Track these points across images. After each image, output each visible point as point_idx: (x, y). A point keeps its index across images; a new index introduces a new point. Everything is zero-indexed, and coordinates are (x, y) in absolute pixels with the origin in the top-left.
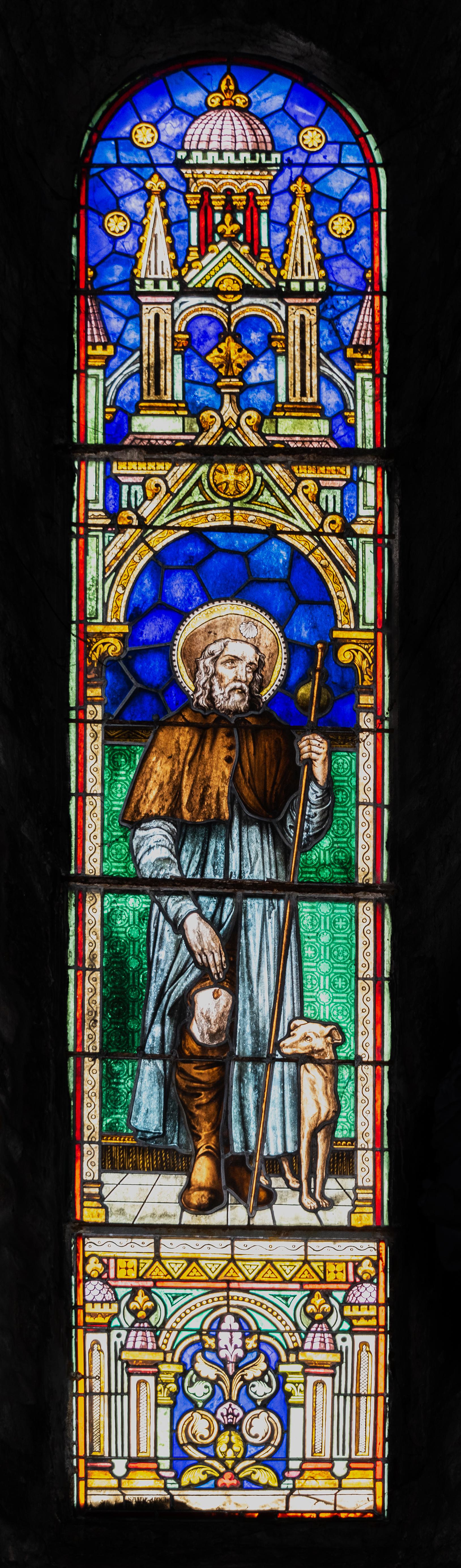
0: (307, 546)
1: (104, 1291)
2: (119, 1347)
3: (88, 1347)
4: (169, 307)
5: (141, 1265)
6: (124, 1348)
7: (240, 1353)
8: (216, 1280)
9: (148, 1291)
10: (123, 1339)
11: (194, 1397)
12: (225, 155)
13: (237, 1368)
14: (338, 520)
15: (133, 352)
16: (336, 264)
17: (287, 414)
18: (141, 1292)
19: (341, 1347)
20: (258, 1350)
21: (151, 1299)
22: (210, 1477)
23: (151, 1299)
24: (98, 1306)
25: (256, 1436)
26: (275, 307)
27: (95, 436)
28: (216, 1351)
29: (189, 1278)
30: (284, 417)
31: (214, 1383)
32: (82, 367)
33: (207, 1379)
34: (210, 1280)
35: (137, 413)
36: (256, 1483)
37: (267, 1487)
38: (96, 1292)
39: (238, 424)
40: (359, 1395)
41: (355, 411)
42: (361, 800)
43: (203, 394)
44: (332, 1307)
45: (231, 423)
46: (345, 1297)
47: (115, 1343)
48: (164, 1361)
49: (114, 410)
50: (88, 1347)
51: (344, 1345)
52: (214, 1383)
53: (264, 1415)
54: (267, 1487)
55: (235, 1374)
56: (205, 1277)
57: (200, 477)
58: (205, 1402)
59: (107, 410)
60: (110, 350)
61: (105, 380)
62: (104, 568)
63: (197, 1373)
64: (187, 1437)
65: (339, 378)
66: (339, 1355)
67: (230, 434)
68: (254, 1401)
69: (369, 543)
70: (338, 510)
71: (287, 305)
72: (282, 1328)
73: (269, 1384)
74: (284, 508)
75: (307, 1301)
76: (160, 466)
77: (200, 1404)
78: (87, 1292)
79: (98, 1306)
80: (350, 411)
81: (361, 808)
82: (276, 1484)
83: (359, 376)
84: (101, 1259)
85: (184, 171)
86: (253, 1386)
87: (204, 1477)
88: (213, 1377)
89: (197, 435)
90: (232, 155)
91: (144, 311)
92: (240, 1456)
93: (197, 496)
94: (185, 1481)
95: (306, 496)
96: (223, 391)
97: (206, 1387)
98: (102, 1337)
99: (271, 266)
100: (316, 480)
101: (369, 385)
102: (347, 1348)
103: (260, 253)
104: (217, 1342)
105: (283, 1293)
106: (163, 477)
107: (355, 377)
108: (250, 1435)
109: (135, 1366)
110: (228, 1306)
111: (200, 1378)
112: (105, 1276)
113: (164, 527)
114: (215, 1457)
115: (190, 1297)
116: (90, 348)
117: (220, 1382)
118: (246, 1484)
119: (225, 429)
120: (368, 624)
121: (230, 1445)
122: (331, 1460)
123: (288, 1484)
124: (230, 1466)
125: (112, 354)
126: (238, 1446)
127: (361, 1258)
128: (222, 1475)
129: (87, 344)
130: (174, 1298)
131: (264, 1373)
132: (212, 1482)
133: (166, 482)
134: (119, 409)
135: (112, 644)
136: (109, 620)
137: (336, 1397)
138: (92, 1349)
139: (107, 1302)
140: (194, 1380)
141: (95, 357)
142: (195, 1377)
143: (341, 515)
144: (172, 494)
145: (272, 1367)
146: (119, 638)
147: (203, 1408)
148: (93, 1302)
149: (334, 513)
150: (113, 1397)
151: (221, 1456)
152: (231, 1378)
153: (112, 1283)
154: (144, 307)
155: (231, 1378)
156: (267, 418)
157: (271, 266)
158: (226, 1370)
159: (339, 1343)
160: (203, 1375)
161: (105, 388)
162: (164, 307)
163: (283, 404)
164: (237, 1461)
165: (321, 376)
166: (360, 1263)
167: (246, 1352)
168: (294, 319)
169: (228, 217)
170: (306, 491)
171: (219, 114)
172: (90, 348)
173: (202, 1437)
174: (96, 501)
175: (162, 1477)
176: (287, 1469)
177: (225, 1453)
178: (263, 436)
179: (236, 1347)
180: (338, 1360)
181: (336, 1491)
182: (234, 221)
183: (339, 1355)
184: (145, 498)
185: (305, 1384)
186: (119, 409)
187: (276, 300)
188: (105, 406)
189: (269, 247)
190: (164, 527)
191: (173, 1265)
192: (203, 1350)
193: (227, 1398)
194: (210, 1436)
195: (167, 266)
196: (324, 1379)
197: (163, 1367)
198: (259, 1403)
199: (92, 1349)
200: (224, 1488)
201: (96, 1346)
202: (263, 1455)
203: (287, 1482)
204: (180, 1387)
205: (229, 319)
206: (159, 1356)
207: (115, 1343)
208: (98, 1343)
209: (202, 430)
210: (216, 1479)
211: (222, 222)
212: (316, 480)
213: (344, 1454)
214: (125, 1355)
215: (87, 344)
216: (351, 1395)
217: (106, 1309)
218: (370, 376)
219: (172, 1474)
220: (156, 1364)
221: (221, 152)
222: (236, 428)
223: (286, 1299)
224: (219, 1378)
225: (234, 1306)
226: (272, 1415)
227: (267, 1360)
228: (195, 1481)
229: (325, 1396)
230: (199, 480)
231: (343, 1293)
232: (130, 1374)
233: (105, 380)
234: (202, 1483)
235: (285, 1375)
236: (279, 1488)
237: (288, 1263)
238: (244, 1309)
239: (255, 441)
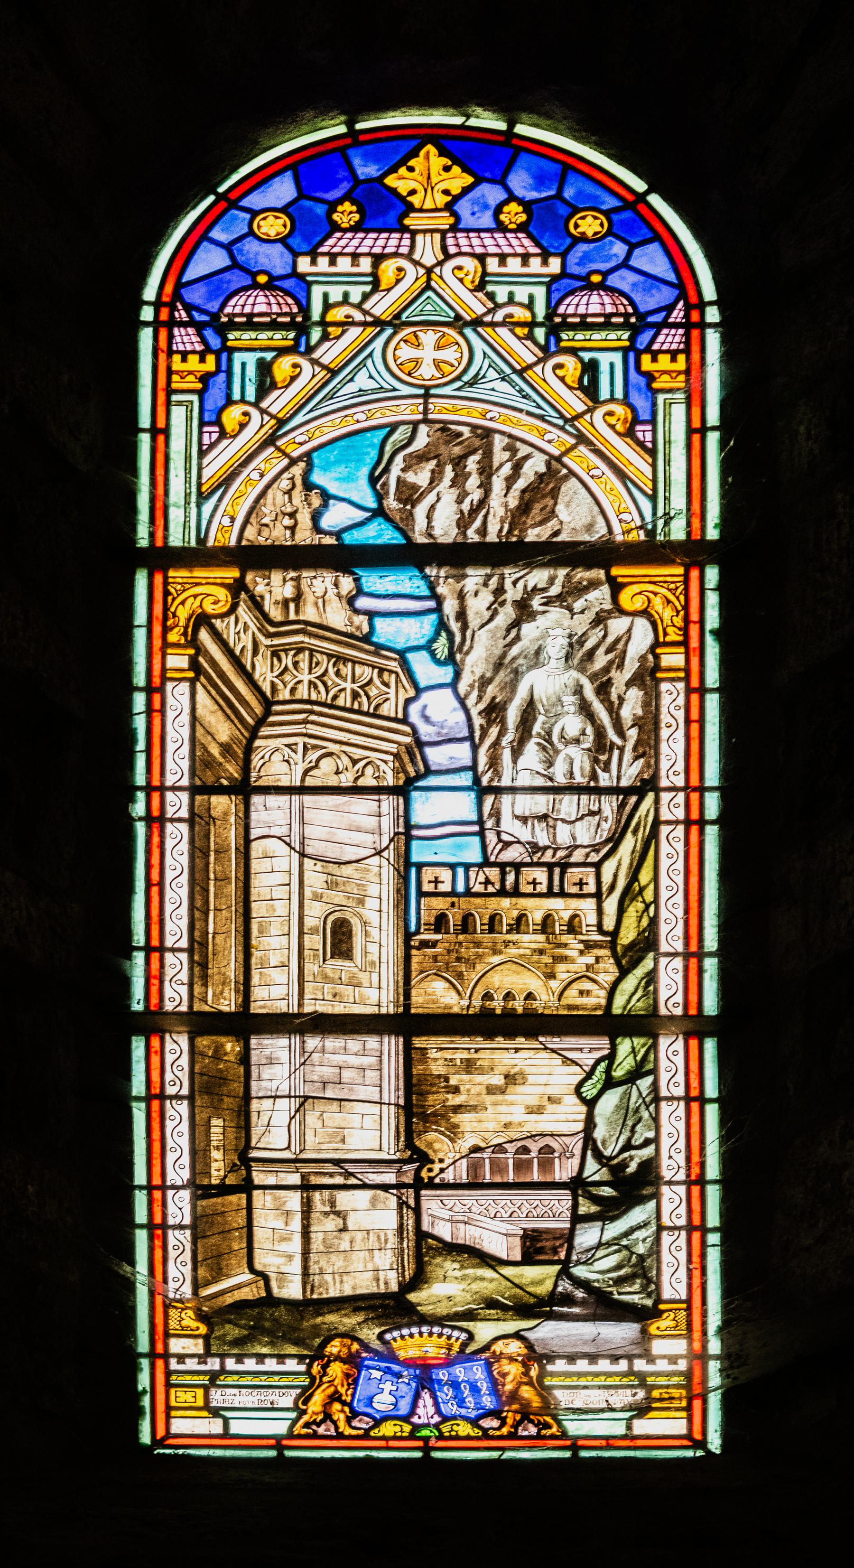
70: (619, 394)
116: (177, 358)
149: (612, 399)
172: (177, 358)
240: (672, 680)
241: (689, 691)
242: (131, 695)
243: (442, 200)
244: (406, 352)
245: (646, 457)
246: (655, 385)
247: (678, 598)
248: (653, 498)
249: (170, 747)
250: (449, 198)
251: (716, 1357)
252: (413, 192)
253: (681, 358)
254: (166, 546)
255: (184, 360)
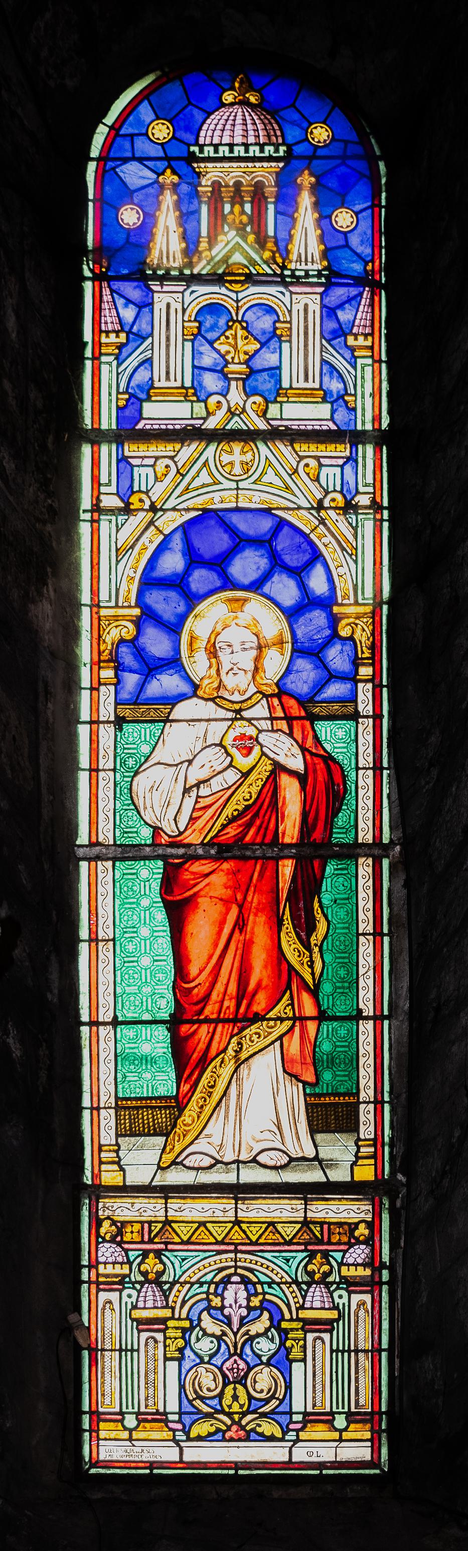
0: (309, 526)
1: (116, 1254)
2: (129, 1307)
3: (100, 1306)
4: (180, 295)
5: (153, 1228)
6: (135, 1307)
7: (244, 1312)
8: (222, 1243)
9: (158, 1254)
10: (134, 1299)
11: (199, 1352)
12: (236, 149)
13: (242, 1324)
14: (339, 497)
15: (144, 339)
16: (340, 253)
17: (290, 399)
18: (151, 1255)
19: (338, 1304)
20: (262, 1308)
21: (162, 1262)
22: (218, 1430)
23: (162, 1262)
24: (110, 1266)
25: (262, 1391)
26: (280, 296)
27: (108, 421)
28: (223, 1307)
29: (197, 1241)
30: (288, 402)
31: (219, 1339)
32: (97, 354)
33: (213, 1335)
34: (217, 1243)
35: (149, 399)
36: (262, 1434)
37: (272, 1438)
38: (108, 1254)
39: (244, 410)
40: (357, 1351)
41: (355, 395)
42: (360, 766)
43: (211, 382)
44: (332, 1267)
45: (237, 408)
46: (343, 1257)
47: (126, 1303)
48: (173, 1318)
49: (127, 396)
50: (100, 1306)
51: (341, 1302)
52: (219, 1339)
53: (266, 1370)
54: (272, 1438)
55: (239, 1330)
56: (213, 1240)
57: (207, 460)
58: (212, 1356)
59: (120, 396)
60: (123, 337)
61: (119, 365)
62: (117, 550)
63: (204, 1330)
64: (195, 1392)
65: (341, 364)
66: (336, 1312)
67: (236, 418)
68: (259, 1357)
69: (369, 519)
70: (338, 488)
71: (291, 293)
72: (278, 1280)
73: (272, 1340)
74: (288, 488)
75: (308, 1261)
76: (170, 447)
77: (206, 1359)
78: (100, 1254)
79: (110, 1266)
80: (351, 395)
81: (361, 772)
82: (280, 1436)
83: (360, 362)
84: (114, 1223)
85: (195, 165)
86: (258, 1343)
87: (213, 1429)
88: (219, 1333)
89: (205, 419)
90: (242, 149)
91: (156, 299)
92: (245, 1409)
93: (204, 478)
94: (193, 1434)
95: (308, 474)
96: (230, 376)
97: (212, 1342)
98: (114, 1296)
99: (277, 255)
100: (317, 458)
101: (369, 370)
102: (344, 1304)
103: (265, 242)
104: (222, 1301)
105: (284, 1254)
106: (172, 458)
107: (355, 362)
108: (255, 1390)
109: (144, 1324)
110: (236, 1267)
111: (205, 1334)
112: (119, 1239)
113: (174, 509)
114: (222, 1412)
115: (198, 1259)
116: (103, 335)
117: (224, 1337)
118: (252, 1434)
119: (231, 413)
120: (367, 599)
121: (235, 1398)
122: (332, 1414)
123: (291, 1436)
124: (237, 1420)
125: (125, 341)
126: (243, 1398)
127: (356, 1220)
128: (229, 1428)
129: (101, 331)
130: (183, 1260)
131: (268, 1330)
132: (220, 1434)
133: (175, 463)
134: (132, 396)
135: (125, 627)
136: (120, 604)
137: (334, 1354)
138: (104, 1309)
139: (118, 1263)
140: (200, 1336)
141: (107, 345)
142: (201, 1333)
143: (341, 492)
144: (182, 475)
145: (275, 1323)
146: (132, 621)
147: (209, 1363)
148: (105, 1263)
149: (335, 491)
150: (123, 1353)
151: (227, 1410)
152: (235, 1334)
153: (126, 1246)
154: (155, 295)
155: (235, 1334)
156: (272, 402)
157: (277, 255)
158: (229, 1324)
159: (337, 1300)
160: (209, 1331)
161: (118, 374)
162: (175, 295)
163: (287, 389)
164: (244, 1414)
165: (323, 361)
166: (356, 1225)
167: (249, 1309)
168: (298, 307)
169: (237, 208)
170: (307, 470)
171: (231, 110)
172: (103, 335)
173: (209, 1390)
174: (109, 484)
175: (170, 1429)
176: (291, 1422)
177: (230, 1407)
178: (267, 420)
179: (240, 1306)
180: (336, 1317)
181: (336, 1444)
182: (243, 212)
183: (336, 1312)
184: (156, 479)
185: (305, 1339)
186: (132, 396)
187: (282, 289)
188: (118, 393)
189: (275, 237)
190: (174, 509)
191: (182, 1229)
192: (208, 1309)
193: (232, 1352)
194: (216, 1388)
195: (179, 255)
196: (323, 1335)
197: (170, 1324)
198: (264, 1359)
199: (104, 1309)
200: (231, 1440)
201: (108, 1306)
202: (267, 1409)
203: (291, 1433)
204: (187, 1343)
205: (238, 307)
206: (167, 1313)
207: (126, 1303)
208: (110, 1302)
209: (209, 414)
210: (224, 1432)
211: (232, 212)
212: (317, 458)
213: (343, 1408)
214: (137, 1314)
215: (101, 331)
216: (349, 1351)
217: (118, 1270)
218: (370, 361)
219: (180, 1426)
220: (164, 1321)
221: (231, 146)
222: (241, 413)
223: (288, 1261)
224: (224, 1333)
225: (241, 1267)
226: (274, 1370)
227: (271, 1319)
228: (204, 1434)
229: (323, 1354)
230: (205, 464)
231: (341, 1254)
232: (139, 1331)
233: (119, 365)
234: (210, 1434)
235: (286, 1331)
236: (282, 1440)
237: (289, 1225)
238: (251, 1270)
239: (262, 425)
240: (366, 1140)
241: (374, 361)
242: (82, 1112)
243: (243, 357)
244: (226, 458)
245: (351, 529)
246: (356, 354)
247: (368, 627)
248: (356, 562)
249: (101, 989)
250: (248, 357)
251: (385, 362)
252: (228, 352)
253: (370, 338)
254: (99, 429)
255: (107, 336)
